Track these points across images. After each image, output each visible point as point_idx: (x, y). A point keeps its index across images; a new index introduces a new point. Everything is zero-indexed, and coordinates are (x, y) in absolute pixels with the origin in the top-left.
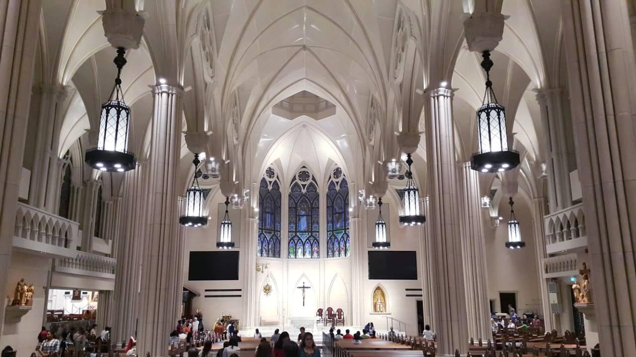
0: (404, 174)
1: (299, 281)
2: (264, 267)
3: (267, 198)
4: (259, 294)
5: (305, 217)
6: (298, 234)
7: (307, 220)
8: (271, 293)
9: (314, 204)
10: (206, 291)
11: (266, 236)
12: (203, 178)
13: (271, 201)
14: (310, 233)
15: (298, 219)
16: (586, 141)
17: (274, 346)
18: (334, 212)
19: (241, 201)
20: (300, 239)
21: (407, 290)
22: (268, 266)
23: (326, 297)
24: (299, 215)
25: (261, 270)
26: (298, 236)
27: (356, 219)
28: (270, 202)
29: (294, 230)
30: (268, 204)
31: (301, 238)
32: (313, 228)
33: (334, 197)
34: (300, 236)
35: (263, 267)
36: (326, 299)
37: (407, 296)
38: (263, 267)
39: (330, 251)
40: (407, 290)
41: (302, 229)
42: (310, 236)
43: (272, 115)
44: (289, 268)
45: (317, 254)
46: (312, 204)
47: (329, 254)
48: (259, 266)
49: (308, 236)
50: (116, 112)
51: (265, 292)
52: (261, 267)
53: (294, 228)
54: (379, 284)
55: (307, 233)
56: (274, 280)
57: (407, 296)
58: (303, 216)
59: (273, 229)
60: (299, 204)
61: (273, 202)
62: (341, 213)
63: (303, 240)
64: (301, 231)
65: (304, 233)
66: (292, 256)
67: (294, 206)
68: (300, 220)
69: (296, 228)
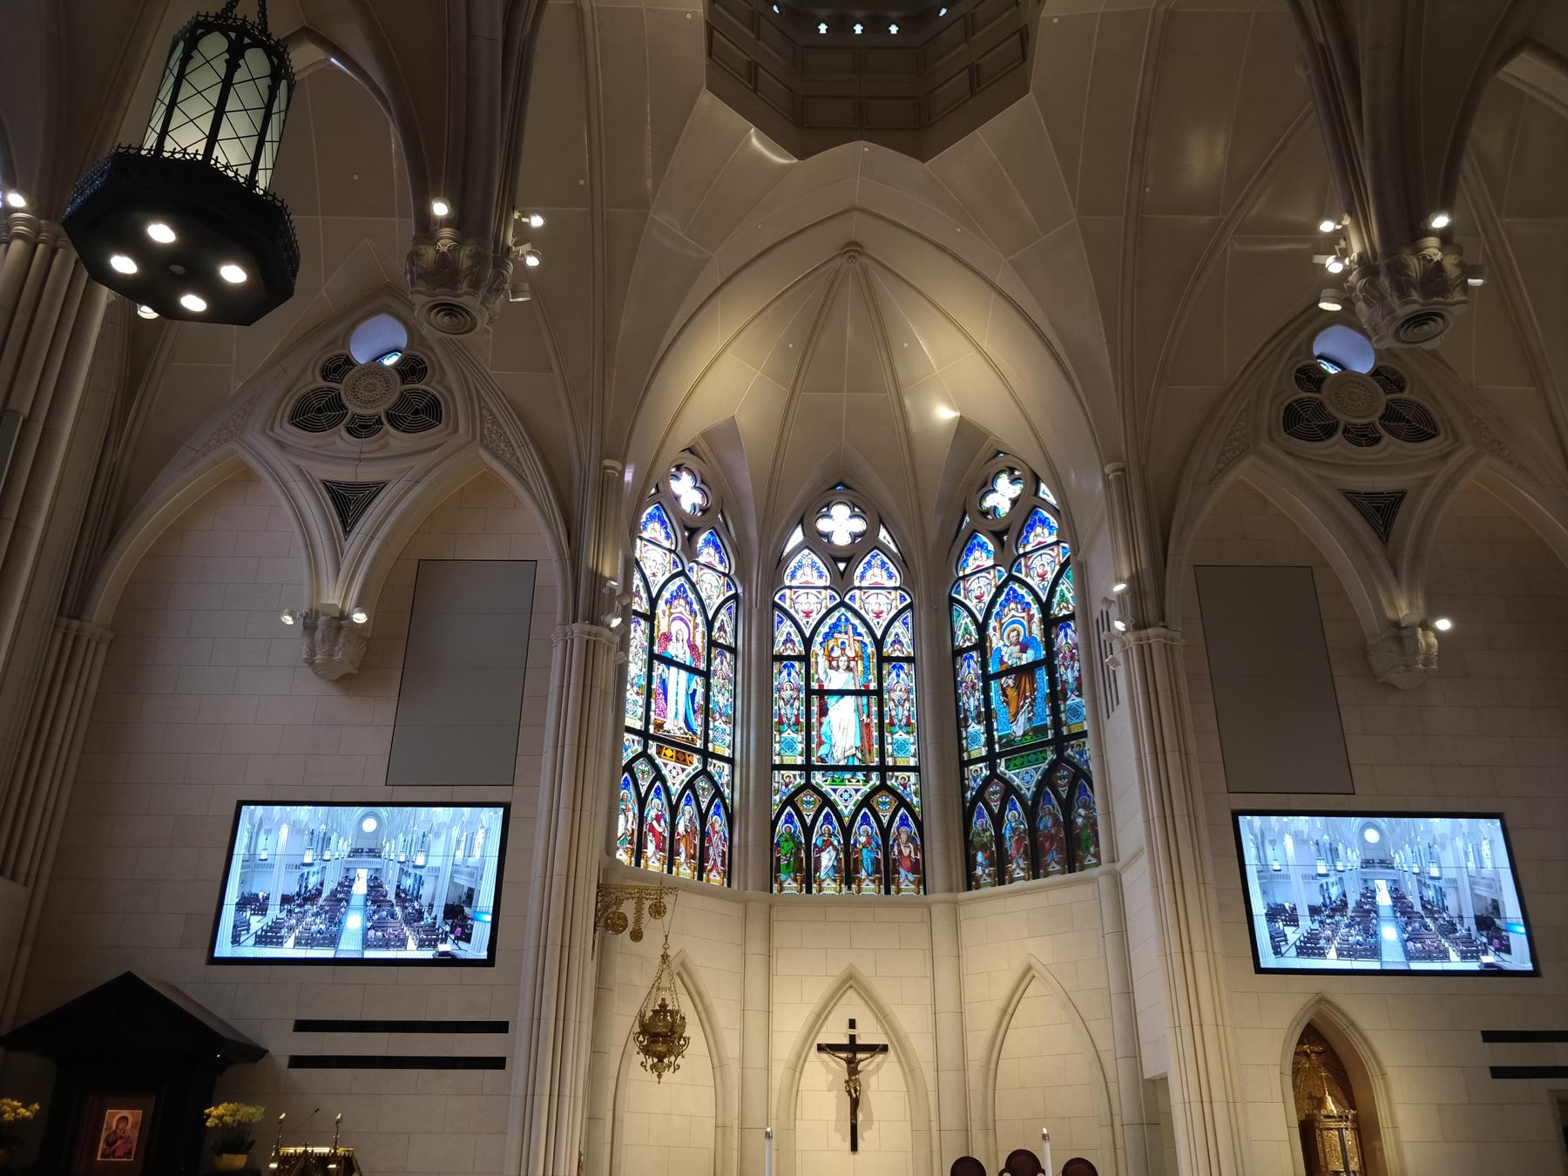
0: (1375, 418)
1: (821, 1017)
2: (647, 904)
3: (673, 598)
4: (613, 1071)
5: (849, 701)
6: (818, 778)
7: (858, 710)
8: (680, 1060)
9: (889, 640)
10: (302, 1026)
11: (665, 771)
12: (349, 430)
13: (693, 612)
14: (874, 775)
15: (815, 709)
16: (1197, 980)
17: (629, 489)
18: (991, 670)
19: (478, 259)
20: (826, 801)
21: (1489, 1036)
22: (668, 900)
23: (975, 1100)
24: (823, 693)
25: (630, 927)
26: (817, 791)
27: (1151, 631)
28: (687, 616)
29: (800, 761)
30: (678, 625)
31: (833, 797)
32: (889, 748)
33: (987, 599)
34: (826, 788)
35: (639, 911)
36: (976, 1115)
37: (1498, 1073)
38: (639, 911)
39: (980, 857)
40: (1489, 1036)
41: (838, 757)
42: (875, 791)
43: (707, 99)
44: (776, 941)
45: (911, 877)
46: (879, 644)
47: (979, 871)
48: (619, 902)
49: (866, 789)
50: (224, 44)
51: (646, 1051)
52: (628, 908)
53: (800, 747)
54: (1322, 999)
55: (860, 775)
56: (696, 995)
57: (1498, 1073)
58: (842, 693)
59: (699, 744)
60: (819, 639)
61: (700, 619)
62: (1030, 669)
63: (841, 807)
64: (831, 762)
65: (848, 776)
66: (791, 886)
67: (800, 648)
68: (824, 711)
69: (808, 752)
